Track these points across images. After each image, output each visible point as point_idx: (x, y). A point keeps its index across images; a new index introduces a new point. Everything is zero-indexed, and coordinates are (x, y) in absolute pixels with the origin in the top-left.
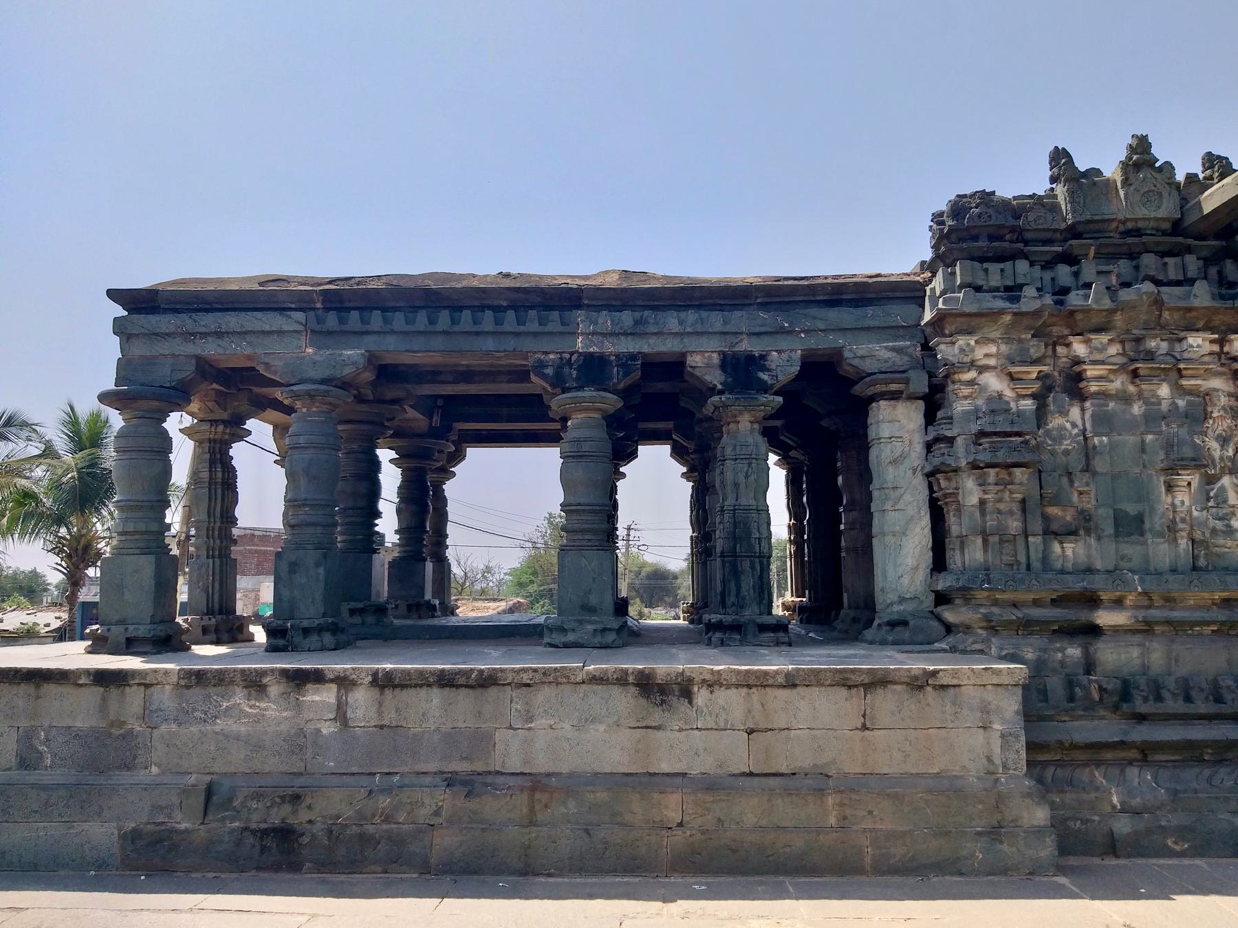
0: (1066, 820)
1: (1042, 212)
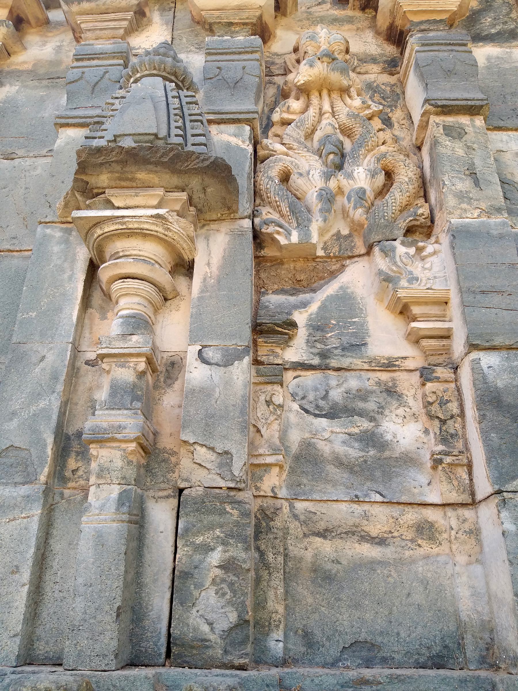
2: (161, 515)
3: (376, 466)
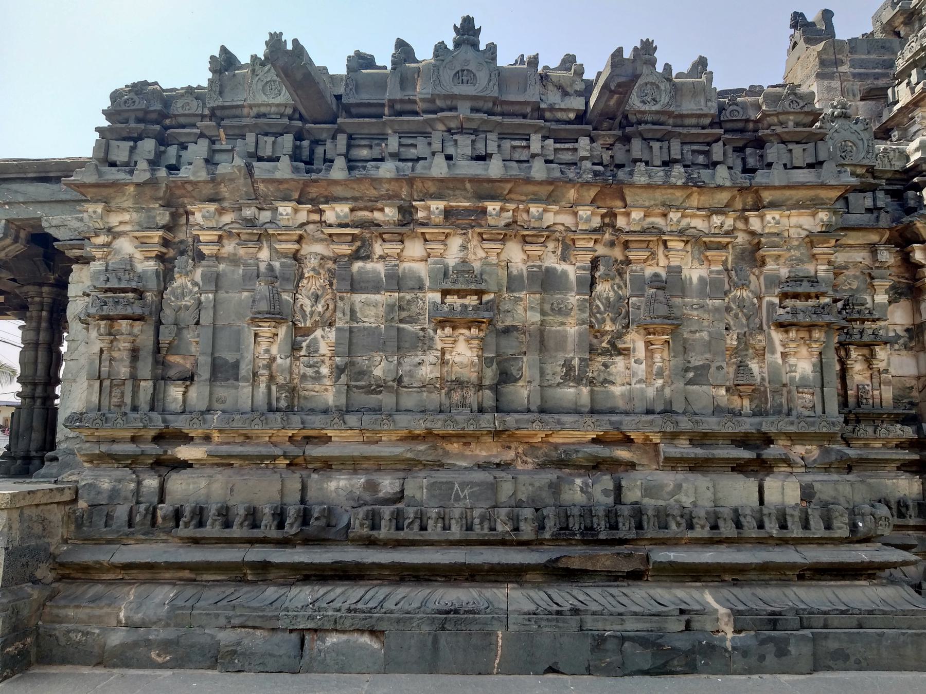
0: (69, 632)
1: (189, 99)
2: (274, 388)
3: (318, 377)
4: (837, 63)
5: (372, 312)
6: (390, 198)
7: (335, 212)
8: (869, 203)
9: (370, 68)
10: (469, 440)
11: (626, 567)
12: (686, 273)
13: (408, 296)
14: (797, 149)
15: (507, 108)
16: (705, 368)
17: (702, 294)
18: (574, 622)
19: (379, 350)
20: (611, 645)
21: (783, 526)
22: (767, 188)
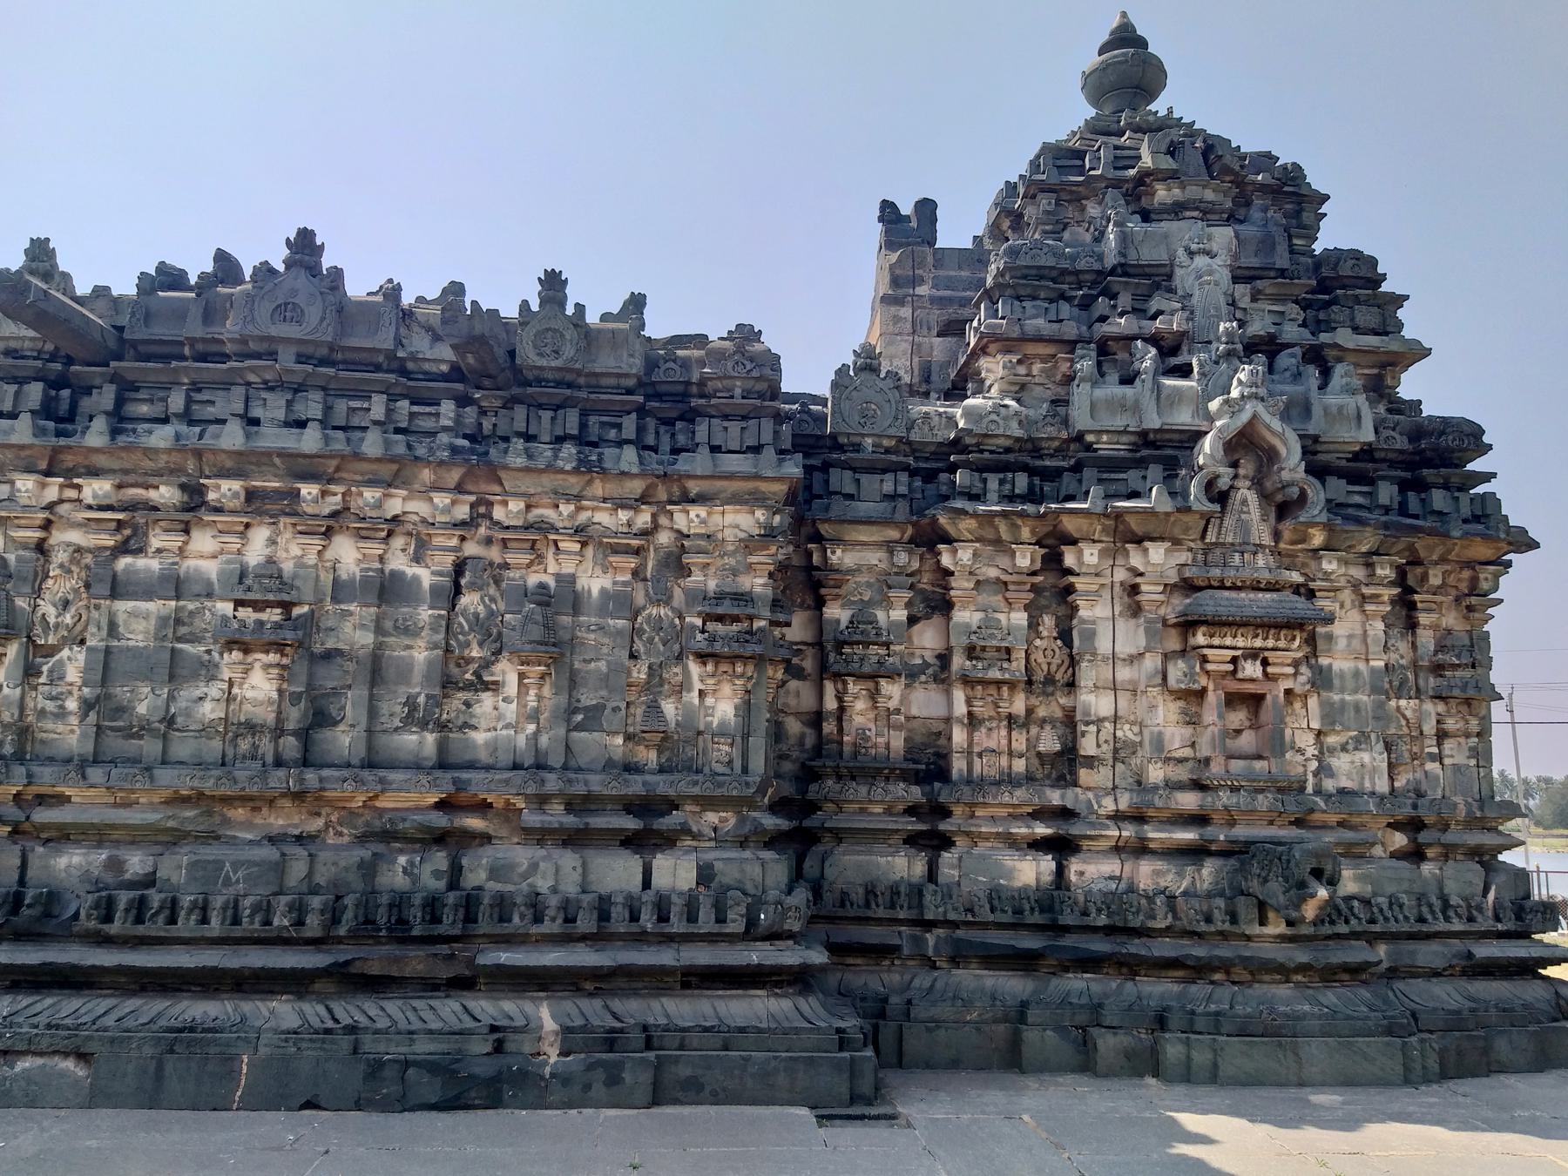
3: (62, 714)
4: (915, 281)
5: (140, 625)
6: (172, 472)
7: (96, 489)
8: (888, 487)
9: (174, 289)
10: (258, 804)
11: (445, 972)
12: (583, 582)
13: (191, 606)
14: (734, 427)
15: (349, 356)
16: (599, 708)
17: (603, 611)
18: (345, 1042)
19: (146, 678)
20: (388, 1073)
21: (663, 918)
22: (690, 477)
